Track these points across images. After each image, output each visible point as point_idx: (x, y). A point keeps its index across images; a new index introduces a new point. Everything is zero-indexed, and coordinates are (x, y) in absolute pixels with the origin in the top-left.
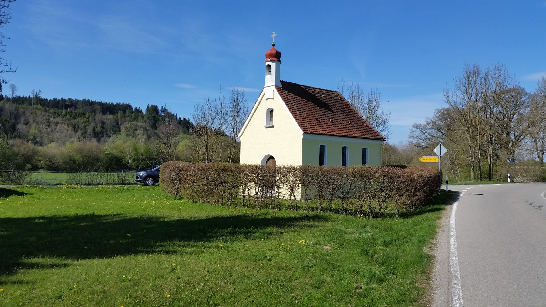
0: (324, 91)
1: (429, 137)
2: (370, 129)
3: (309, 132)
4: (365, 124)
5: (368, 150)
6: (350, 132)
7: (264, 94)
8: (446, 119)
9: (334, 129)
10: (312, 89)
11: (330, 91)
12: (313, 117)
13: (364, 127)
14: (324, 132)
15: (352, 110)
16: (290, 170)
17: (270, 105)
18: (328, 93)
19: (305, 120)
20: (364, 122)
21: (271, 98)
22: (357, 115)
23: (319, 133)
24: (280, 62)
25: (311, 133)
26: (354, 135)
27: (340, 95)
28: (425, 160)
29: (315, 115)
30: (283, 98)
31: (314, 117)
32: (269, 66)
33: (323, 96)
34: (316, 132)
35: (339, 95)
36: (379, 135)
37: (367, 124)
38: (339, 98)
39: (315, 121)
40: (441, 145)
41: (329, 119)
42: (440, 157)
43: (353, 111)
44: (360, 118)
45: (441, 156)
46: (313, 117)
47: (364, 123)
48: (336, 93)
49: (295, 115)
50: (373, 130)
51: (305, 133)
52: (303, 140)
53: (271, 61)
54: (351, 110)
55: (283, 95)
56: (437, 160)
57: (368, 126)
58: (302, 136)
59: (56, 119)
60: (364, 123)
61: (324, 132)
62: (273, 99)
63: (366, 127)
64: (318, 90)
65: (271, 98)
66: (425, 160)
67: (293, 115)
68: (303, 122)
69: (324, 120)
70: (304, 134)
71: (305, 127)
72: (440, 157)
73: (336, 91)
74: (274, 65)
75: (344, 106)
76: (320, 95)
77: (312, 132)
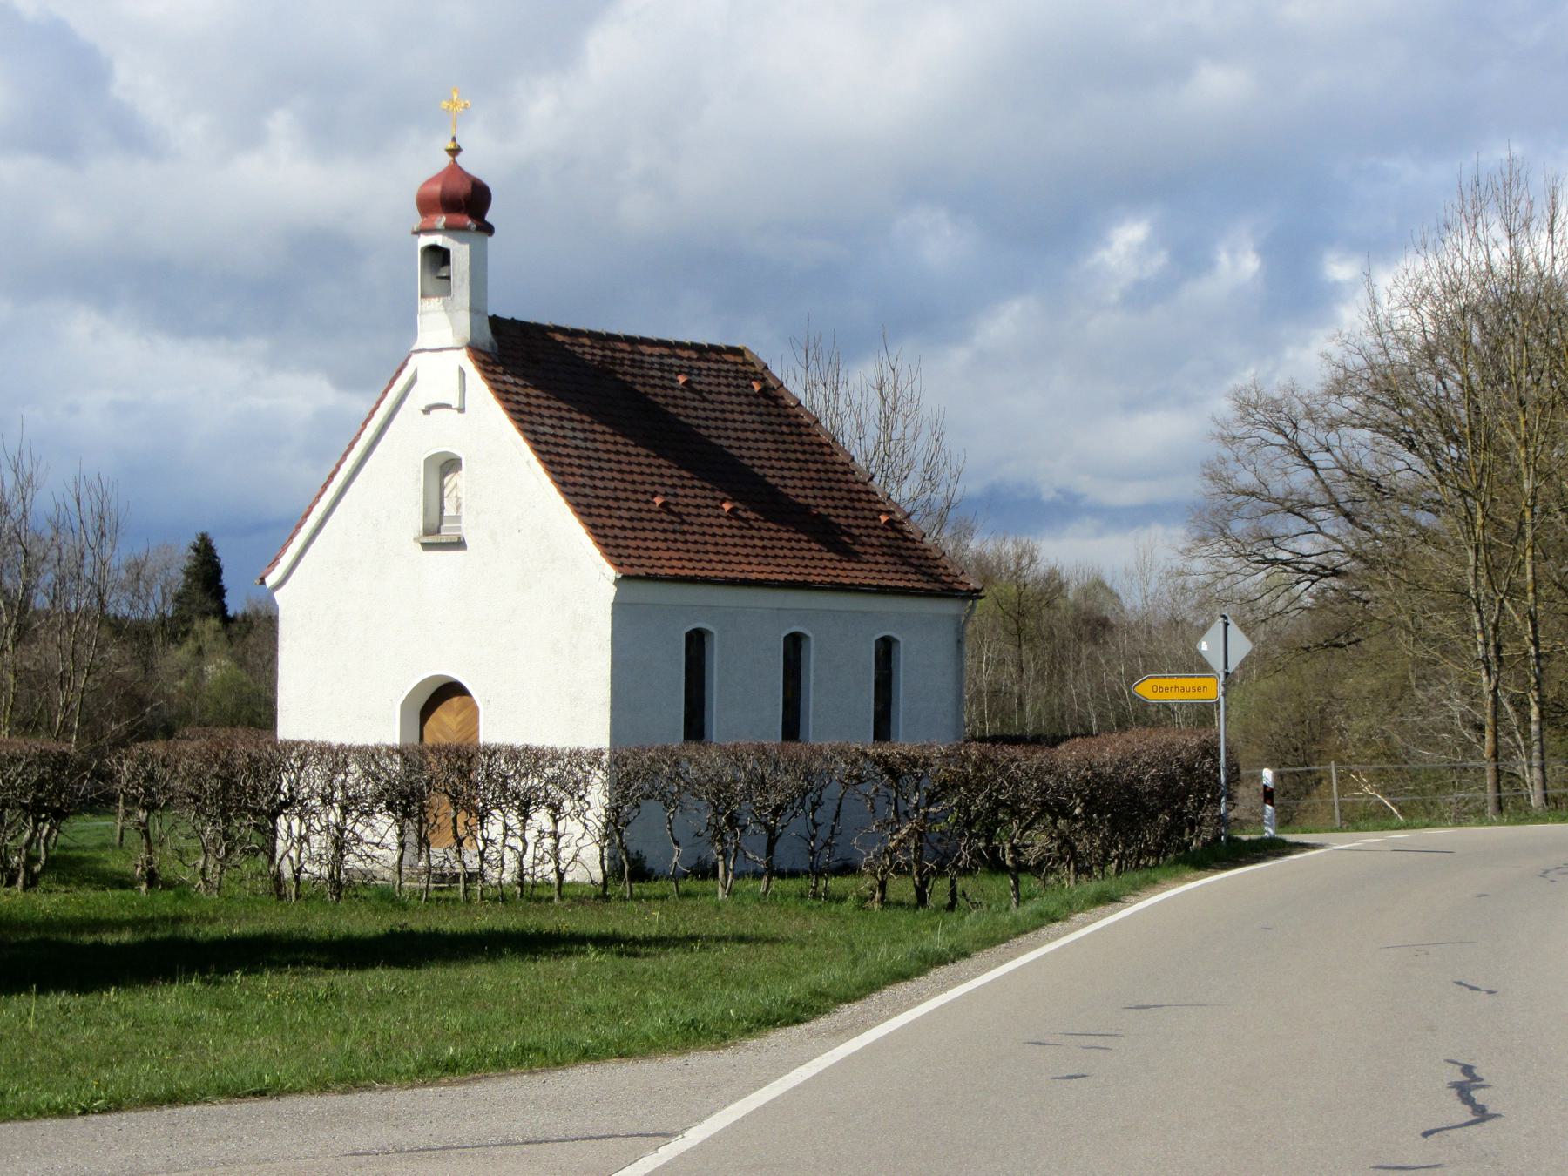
0: (685, 354)
1: (1344, 490)
2: (909, 544)
3: (641, 572)
4: (883, 518)
5: (902, 645)
6: (816, 563)
7: (413, 380)
8: (1466, 343)
9: (745, 551)
10: (626, 347)
11: (712, 348)
12: (648, 497)
13: (879, 532)
14: (703, 569)
15: (821, 445)
16: (334, 757)
17: (445, 434)
18: (702, 364)
19: (618, 513)
20: (880, 506)
21: (448, 406)
22: (845, 473)
23: (682, 573)
24: (488, 229)
25: (649, 578)
26: (838, 576)
27: (759, 368)
28: (1160, 689)
29: (657, 488)
30: (510, 411)
31: (654, 495)
32: (438, 256)
33: (682, 379)
34: (672, 572)
35: (752, 369)
36: (951, 570)
37: (891, 517)
38: (757, 387)
39: (658, 517)
40: (1230, 621)
41: (718, 503)
42: (1222, 675)
43: (826, 450)
44: (859, 487)
45: (1227, 674)
46: (648, 497)
47: (880, 512)
48: (739, 360)
49: (576, 489)
50: (922, 546)
51: (624, 580)
52: (613, 613)
53: (449, 229)
54: (815, 448)
55: (509, 396)
56: (1210, 689)
57: (899, 526)
58: (610, 592)
59: (152, 615)
60: (880, 512)
61: (703, 569)
62: (461, 410)
63: (891, 534)
64: (657, 351)
65: (448, 406)
66: (1160, 689)
67: (565, 494)
68: (609, 522)
69: (698, 506)
70: (625, 582)
71: (620, 551)
72: (1222, 679)
73: (738, 345)
74: (460, 252)
75: (785, 429)
76: (669, 376)
77: (652, 571)
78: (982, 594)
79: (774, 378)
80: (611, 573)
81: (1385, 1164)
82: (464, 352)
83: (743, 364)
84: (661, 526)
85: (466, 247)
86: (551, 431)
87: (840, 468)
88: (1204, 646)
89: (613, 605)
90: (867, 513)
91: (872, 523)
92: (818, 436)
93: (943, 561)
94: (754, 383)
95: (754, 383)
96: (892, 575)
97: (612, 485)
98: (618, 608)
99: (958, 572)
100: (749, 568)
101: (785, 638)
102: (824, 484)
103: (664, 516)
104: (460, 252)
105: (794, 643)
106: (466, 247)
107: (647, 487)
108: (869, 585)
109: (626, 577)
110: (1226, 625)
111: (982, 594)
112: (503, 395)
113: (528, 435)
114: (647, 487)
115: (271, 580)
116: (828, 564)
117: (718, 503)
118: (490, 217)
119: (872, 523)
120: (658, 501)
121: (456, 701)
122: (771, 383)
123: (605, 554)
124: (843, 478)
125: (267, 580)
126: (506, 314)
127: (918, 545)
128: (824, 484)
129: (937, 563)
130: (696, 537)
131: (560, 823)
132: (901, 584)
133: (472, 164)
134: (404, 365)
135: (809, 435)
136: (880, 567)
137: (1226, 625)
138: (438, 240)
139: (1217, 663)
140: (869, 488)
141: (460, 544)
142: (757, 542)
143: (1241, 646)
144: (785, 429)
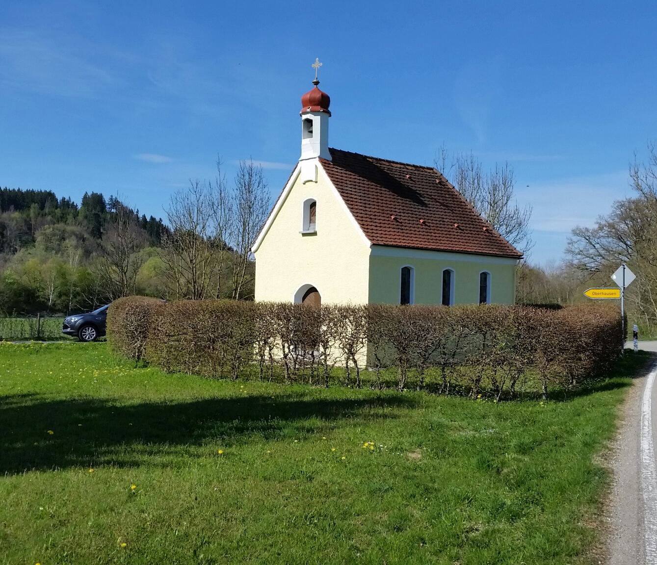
1: (603, 252)
4: (485, 229)
10: (387, 164)
11: (421, 167)
16: (346, 312)
21: (311, 181)
23: (400, 244)
27: (439, 175)
28: (596, 294)
30: (333, 181)
31: (391, 215)
32: (309, 122)
38: (438, 181)
42: (622, 288)
45: (624, 288)
47: (483, 226)
48: (431, 171)
50: (500, 239)
51: (374, 245)
53: (313, 112)
56: (617, 294)
57: (491, 232)
62: (316, 182)
63: (487, 234)
64: (399, 166)
65: (311, 181)
66: (596, 294)
68: (371, 224)
71: (373, 234)
72: (622, 290)
74: (317, 120)
75: (447, 196)
77: (386, 243)
78: (523, 257)
79: (445, 178)
80: (369, 243)
81: (314, 159)
82: (317, 159)
83: (433, 173)
84: (393, 226)
85: (319, 118)
86: (350, 189)
87: (469, 211)
88: (614, 277)
89: (370, 256)
90: (478, 226)
91: (480, 230)
92: (461, 199)
93: (508, 245)
94: (436, 180)
95: (436, 180)
96: (487, 249)
97: (374, 210)
98: (372, 257)
99: (514, 249)
100: (429, 244)
101: (444, 272)
102: (462, 215)
103: (394, 223)
104: (317, 120)
105: (447, 274)
106: (319, 118)
107: (388, 212)
108: (478, 252)
109: (374, 244)
110: (624, 268)
111: (523, 257)
112: (331, 175)
113: (339, 190)
114: (388, 212)
115: (253, 249)
116: (461, 244)
117: (418, 219)
118: (329, 109)
119: (480, 230)
120: (393, 217)
121: (312, 295)
122: (443, 180)
123: (367, 236)
124: (470, 214)
125: (252, 249)
126: (338, 147)
127: (498, 239)
128: (462, 215)
129: (505, 245)
130: (407, 231)
131: (327, 350)
132: (491, 252)
133: (324, 89)
134: (297, 166)
135: (457, 198)
136: (482, 246)
137: (624, 268)
138: (309, 116)
139: (620, 284)
140: (479, 218)
141: (315, 234)
142: (433, 234)
143: (630, 277)
144: (447, 196)
